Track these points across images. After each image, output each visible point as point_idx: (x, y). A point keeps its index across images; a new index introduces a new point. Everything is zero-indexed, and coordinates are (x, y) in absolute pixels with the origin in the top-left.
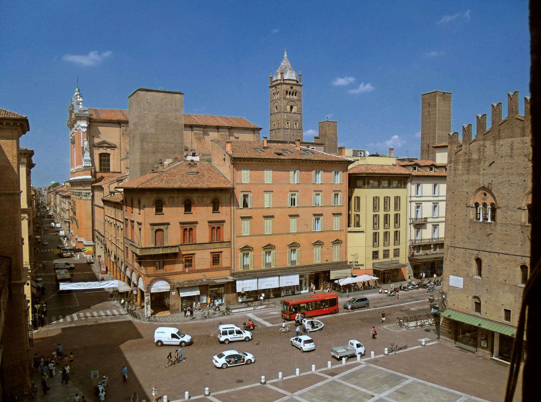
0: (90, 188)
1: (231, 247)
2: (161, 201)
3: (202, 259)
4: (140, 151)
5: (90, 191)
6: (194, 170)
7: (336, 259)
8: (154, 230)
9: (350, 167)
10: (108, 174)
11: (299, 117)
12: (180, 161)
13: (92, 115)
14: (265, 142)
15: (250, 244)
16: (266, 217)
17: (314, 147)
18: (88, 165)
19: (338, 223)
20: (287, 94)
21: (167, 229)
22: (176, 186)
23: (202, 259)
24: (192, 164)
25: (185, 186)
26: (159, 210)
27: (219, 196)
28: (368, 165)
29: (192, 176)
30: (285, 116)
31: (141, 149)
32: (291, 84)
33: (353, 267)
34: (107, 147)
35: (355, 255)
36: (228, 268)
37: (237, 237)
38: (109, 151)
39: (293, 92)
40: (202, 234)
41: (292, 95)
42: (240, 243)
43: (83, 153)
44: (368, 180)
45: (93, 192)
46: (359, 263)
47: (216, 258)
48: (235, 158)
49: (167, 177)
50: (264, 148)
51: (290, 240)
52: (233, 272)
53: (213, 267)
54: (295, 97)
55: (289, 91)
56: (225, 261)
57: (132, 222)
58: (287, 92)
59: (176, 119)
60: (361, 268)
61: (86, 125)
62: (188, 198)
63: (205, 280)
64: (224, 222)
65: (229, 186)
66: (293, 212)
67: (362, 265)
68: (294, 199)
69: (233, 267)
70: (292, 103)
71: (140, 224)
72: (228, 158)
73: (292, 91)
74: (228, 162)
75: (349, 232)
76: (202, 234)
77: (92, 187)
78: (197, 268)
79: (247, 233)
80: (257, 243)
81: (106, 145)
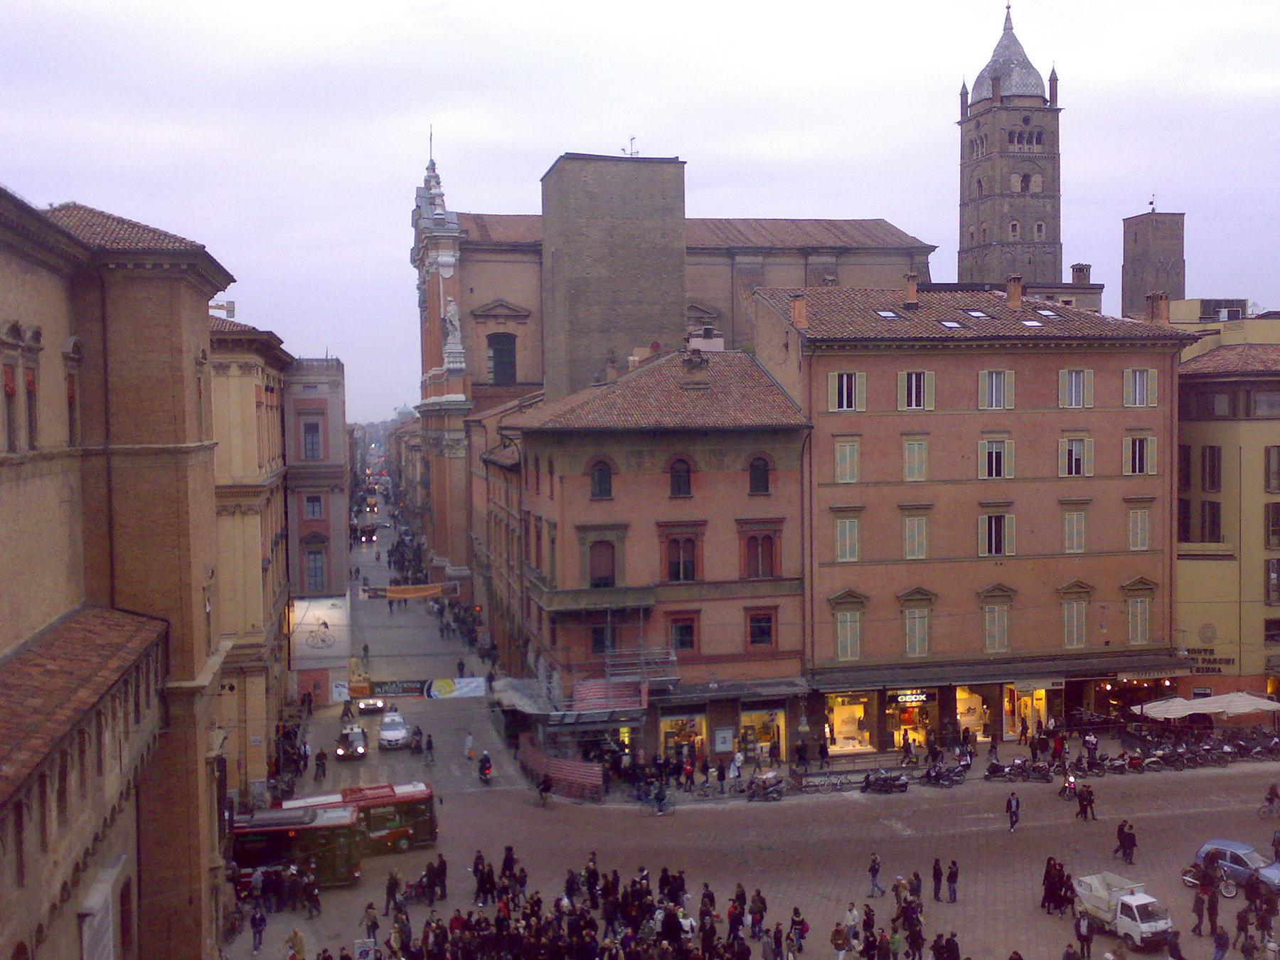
0: (462, 426)
1: (803, 595)
2: (683, 461)
3: (723, 625)
4: (567, 327)
5: (462, 435)
6: (699, 376)
7: (1138, 640)
8: (588, 544)
9: (1188, 353)
10: (512, 389)
11: (1049, 208)
12: (668, 353)
13: (467, 231)
14: (913, 287)
15: (861, 589)
16: (1065, 504)
17: (1073, 299)
18: (458, 366)
19: (1145, 530)
20: (1011, 141)
21: (622, 540)
22: (644, 423)
23: (723, 625)
24: (697, 361)
25: (669, 421)
26: (603, 491)
27: (765, 451)
28: (1251, 346)
29: (693, 394)
30: (1006, 208)
31: (571, 323)
32: (1026, 109)
33: (1206, 671)
34: (507, 317)
35: (1207, 630)
36: (799, 654)
37: (822, 565)
38: (510, 327)
39: (1031, 135)
40: (721, 556)
41: (1030, 142)
42: (826, 584)
43: (446, 334)
44: (1248, 393)
45: (468, 436)
46: (1217, 656)
47: (761, 627)
48: (813, 341)
49: (624, 398)
50: (908, 307)
51: (904, 580)
52: (809, 666)
53: (751, 648)
54: (1036, 148)
55: (1018, 129)
56: (787, 635)
57: (539, 519)
58: (1011, 134)
59: (664, 236)
60: (1226, 670)
61: (452, 260)
62: (679, 451)
63: (713, 686)
64: (781, 521)
65: (799, 419)
66: (1076, 489)
67: (1228, 662)
68: (998, 455)
69: (808, 650)
70: (1027, 168)
71: (554, 526)
72: (794, 339)
73: (1028, 129)
74: (795, 355)
75: (1180, 557)
76: (721, 556)
77: (467, 423)
78: (707, 650)
79: (1079, 546)
80: (881, 585)
81: (506, 312)
